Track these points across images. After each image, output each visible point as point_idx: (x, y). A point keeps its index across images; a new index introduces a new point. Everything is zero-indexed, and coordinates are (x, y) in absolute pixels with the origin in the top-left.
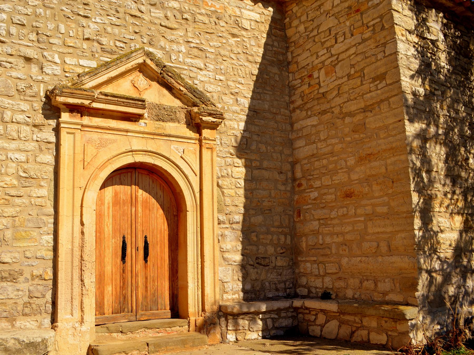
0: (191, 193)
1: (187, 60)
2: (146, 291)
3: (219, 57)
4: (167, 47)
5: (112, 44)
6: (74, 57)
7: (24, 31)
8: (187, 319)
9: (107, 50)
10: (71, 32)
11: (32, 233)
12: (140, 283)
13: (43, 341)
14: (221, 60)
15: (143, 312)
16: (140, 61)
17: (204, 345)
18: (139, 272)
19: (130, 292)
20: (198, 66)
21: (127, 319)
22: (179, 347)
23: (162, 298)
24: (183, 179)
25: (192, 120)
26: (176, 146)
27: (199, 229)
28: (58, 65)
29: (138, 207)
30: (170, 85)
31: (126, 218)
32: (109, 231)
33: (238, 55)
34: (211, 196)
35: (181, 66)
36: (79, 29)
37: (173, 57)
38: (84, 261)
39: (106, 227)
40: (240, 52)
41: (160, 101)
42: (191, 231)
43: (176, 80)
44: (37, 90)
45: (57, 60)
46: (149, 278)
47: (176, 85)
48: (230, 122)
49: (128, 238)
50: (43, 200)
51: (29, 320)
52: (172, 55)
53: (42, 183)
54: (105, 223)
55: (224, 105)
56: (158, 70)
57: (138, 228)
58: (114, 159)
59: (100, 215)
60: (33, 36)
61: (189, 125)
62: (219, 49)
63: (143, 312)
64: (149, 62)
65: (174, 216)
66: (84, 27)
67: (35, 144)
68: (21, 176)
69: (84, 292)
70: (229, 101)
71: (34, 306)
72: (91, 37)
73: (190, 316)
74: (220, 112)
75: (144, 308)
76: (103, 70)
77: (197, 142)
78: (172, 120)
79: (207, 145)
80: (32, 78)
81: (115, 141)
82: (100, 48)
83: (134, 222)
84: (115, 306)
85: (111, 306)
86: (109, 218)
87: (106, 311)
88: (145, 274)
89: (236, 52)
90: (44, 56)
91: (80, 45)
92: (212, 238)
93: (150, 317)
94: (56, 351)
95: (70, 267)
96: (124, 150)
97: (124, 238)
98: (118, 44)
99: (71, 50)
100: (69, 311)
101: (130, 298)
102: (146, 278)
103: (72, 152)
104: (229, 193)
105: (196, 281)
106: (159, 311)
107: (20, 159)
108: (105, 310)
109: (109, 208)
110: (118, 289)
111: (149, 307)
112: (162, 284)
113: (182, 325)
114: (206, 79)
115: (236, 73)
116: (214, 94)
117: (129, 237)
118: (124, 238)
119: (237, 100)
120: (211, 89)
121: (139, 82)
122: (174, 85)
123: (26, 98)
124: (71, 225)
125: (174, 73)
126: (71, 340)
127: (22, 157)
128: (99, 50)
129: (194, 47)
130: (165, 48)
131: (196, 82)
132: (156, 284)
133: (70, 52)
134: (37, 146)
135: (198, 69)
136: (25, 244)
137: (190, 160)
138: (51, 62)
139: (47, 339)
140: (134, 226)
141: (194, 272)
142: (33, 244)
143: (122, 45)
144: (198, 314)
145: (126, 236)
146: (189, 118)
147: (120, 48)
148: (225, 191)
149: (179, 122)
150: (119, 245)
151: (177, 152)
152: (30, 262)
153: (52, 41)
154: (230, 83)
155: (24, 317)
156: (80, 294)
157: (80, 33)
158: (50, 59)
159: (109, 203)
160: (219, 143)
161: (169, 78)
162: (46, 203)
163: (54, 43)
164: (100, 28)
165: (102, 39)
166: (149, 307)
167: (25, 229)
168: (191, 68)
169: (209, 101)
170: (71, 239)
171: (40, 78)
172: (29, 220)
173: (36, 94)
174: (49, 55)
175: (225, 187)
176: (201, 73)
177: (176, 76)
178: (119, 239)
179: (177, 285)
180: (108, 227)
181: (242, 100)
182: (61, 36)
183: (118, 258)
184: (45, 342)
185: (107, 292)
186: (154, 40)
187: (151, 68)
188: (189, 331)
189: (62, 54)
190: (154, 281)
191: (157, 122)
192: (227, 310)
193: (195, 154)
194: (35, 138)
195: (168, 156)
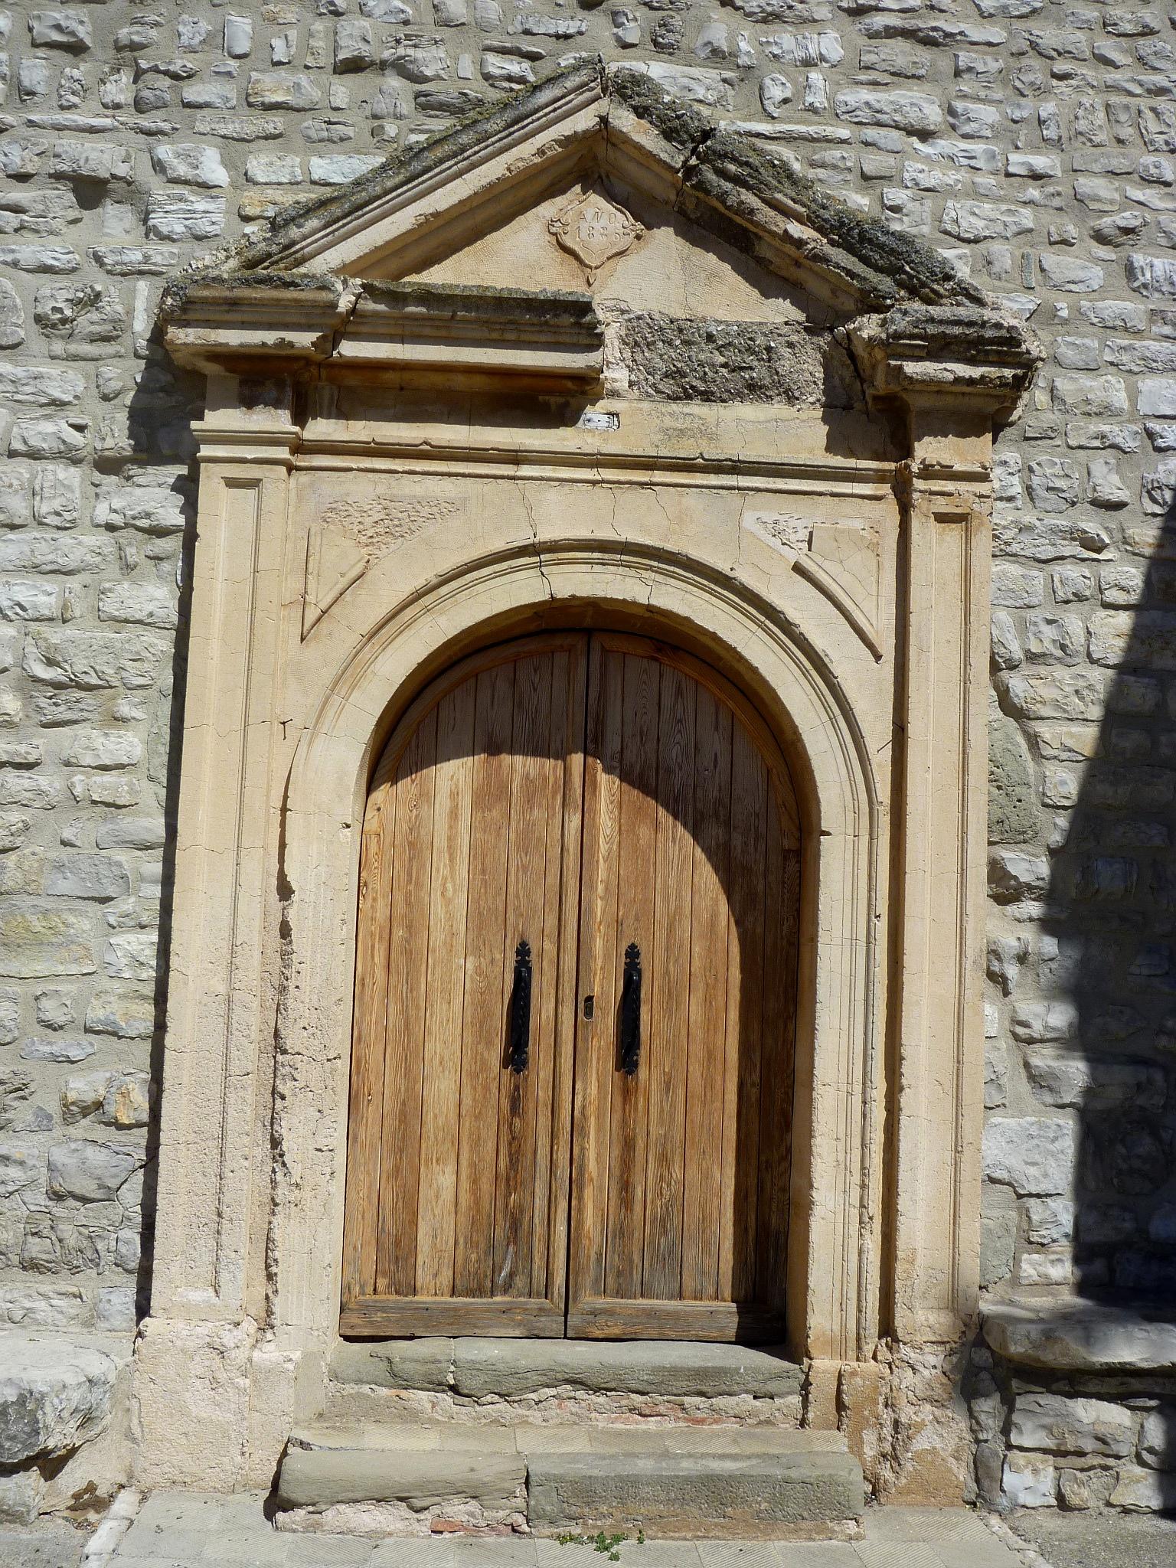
0: (843, 746)
1: (847, 98)
2: (625, 1199)
3: (1033, 61)
4: (744, 46)
5: (467, 67)
6: (288, 149)
7: (80, 70)
8: (800, 1363)
9: (442, 97)
10: (278, 43)
11: (72, 919)
12: (592, 1166)
13: (22, 1401)
14: (1039, 77)
15: (601, 1302)
16: (584, 121)
17: (838, 1519)
18: (591, 1110)
19: (540, 1202)
20: (913, 117)
21: (519, 1324)
22: (693, 1509)
23: (706, 1244)
24: (805, 673)
25: (862, 381)
26: (769, 517)
27: (882, 927)
28: (215, 192)
29: (595, 811)
30: (738, 219)
31: (537, 862)
32: (450, 917)
33: (1141, 41)
34: (955, 758)
35: (812, 130)
36: (319, 26)
37: (776, 93)
38: (284, 1052)
39: (436, 896)
40: (1155, 24)
41: (693, 302)
42: (836, 933)
43: (767, 195)
44: (119, 308)
45: (214, 171)
46: (640, 1144)
47: (766, 215)
48: (1086, 381)
49: (541, 955)
50: (124, 780)
51: (46, 1288)
52: (768, 82)
53: (125, 709)
54: (437, 885)
55: (1054, 295)
56: (673, 155)
57: (591, 911)
58: (444, 590)
59: (411, 844)
60: (120, 88)
61: (848, 407)
62: (1029, 24)
63: (601, 1302)
64: (625, 121)
65: (786, 854)
66: (337, 14)
67: (104, 538)
68: (36, 680)
69: (281, 1193)
70: (1081, 275)
71: (67, 1231)
72: (365, 50)
73: (813, 1352)
74: (998, 326)
75: (610, 1280)
76: (389, 184)
77: (885, 489)
78: (754, 390)
79: (941, 500)
80: (102, 264)
81: (455, 507)
82: (411, 97)
83: (572, 883)
84: (467, 1260)
85: (448, 1256)
86: (452, 859)
87: (423, 1277)
88: (624, 1122)
89: (1129, 28)
90: (159, 166)
91: (316, 94)
92: (953, 969)
93: (638, 1329)
94: (134, 1440)
95: (217, 1076)
96: (499, 545)
97: (523, 951)
98: (497, 64)
99: (275, 122)
100: (206, 1270)
101: (539, 1230)
102: (628, 1144)
103: (248, 565)
104: (1070, 743)
105: (856, 1178)
106: (689, 1304)
107: (35, 607)
108: (419, 1272)
109: (454, 814)
110: (486, 1185)
111: (637, 1277)
112: (706, 1175)
113: (771, 1387)
114: (953, 176)
115: (1126, 132)
116: (996, 247)
117: (549, 947)
118: (523, 951)
119: (1130, 271)
120: (981, 224)
121: (584, 226)
122: (758, 217)
123: (74, 348)
124: (228, 892)
125: (754, 160)
126: (199, 1402)
127: (43, 596)
128: (406, 107)
129: (890, 33)
130: (734, 54)
131: (896, 195)
132: (677, 1173)
133: (270, 129)
134: (109, 549)
135: (910, 131)
136: (41, 968)
137: (845, 579)
138: (186, 182)
139: (43, 1396)
140: (571, 900)
141: (848, 1135)
142: (74, 969)
143: (515, 67)
144: (859, 1348)
145: (534, 947)
146: (848, 374)
147: (506, 85)
148: (1043, 729)
149: (791, 398)
150: (498, 983)
151: (776, 543)
152: (60, 1044)
153: (193, 92)
154: (1092, 185)
155: (29, 1275)
156: (266, 1200)
157: (319, 43)
158: (182, 170)
159: (454, 795)
160: (1017, 489)
161: (728, 186)
162: (132, 791)
163: (201, 100)
164: (417, 9)
165: (418, 54)
166: (637, 1277)
167: (44, 903)
168: (871, 133)
169: (948, 278)
170: (225, 950)
171: (136, 256)
172: (60, 867)
173: (116, 322)
174: (178, 155)
175: (1045, 712)
176: (924, 148)
177: (766, 174)
178: (498, 956)
179: (785, 1190)
180: (448, 902)
181: (1156, 262)
182: (233, 65)
183: (489, 1043)
184: (30, 1406)
185: (431, 1193)
186: (677, 21)
187: (639, 147)
188: (803, 1423)
189: (234, 145)
190: (664, 1159)
191: (675, 407)
192: (1006, 1348)
193: (874, 548)
194: (103, 514)
195: (723, 566)
